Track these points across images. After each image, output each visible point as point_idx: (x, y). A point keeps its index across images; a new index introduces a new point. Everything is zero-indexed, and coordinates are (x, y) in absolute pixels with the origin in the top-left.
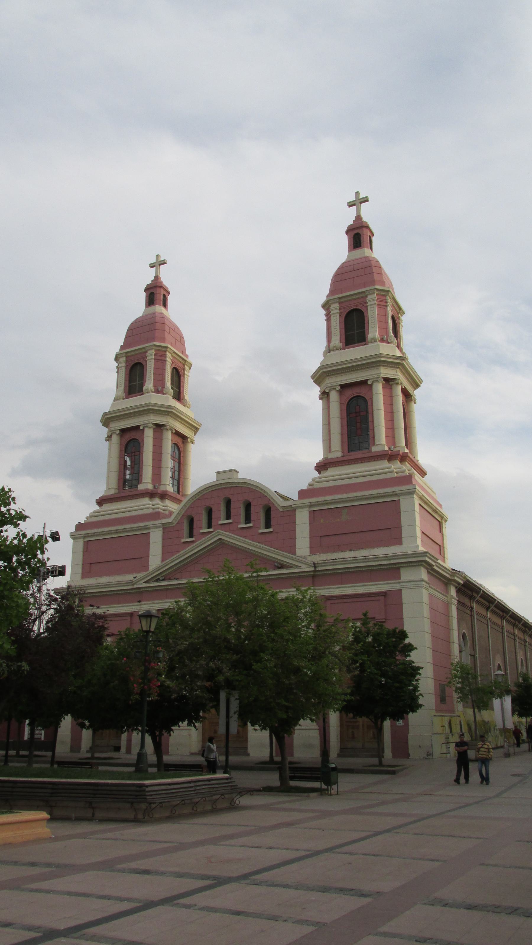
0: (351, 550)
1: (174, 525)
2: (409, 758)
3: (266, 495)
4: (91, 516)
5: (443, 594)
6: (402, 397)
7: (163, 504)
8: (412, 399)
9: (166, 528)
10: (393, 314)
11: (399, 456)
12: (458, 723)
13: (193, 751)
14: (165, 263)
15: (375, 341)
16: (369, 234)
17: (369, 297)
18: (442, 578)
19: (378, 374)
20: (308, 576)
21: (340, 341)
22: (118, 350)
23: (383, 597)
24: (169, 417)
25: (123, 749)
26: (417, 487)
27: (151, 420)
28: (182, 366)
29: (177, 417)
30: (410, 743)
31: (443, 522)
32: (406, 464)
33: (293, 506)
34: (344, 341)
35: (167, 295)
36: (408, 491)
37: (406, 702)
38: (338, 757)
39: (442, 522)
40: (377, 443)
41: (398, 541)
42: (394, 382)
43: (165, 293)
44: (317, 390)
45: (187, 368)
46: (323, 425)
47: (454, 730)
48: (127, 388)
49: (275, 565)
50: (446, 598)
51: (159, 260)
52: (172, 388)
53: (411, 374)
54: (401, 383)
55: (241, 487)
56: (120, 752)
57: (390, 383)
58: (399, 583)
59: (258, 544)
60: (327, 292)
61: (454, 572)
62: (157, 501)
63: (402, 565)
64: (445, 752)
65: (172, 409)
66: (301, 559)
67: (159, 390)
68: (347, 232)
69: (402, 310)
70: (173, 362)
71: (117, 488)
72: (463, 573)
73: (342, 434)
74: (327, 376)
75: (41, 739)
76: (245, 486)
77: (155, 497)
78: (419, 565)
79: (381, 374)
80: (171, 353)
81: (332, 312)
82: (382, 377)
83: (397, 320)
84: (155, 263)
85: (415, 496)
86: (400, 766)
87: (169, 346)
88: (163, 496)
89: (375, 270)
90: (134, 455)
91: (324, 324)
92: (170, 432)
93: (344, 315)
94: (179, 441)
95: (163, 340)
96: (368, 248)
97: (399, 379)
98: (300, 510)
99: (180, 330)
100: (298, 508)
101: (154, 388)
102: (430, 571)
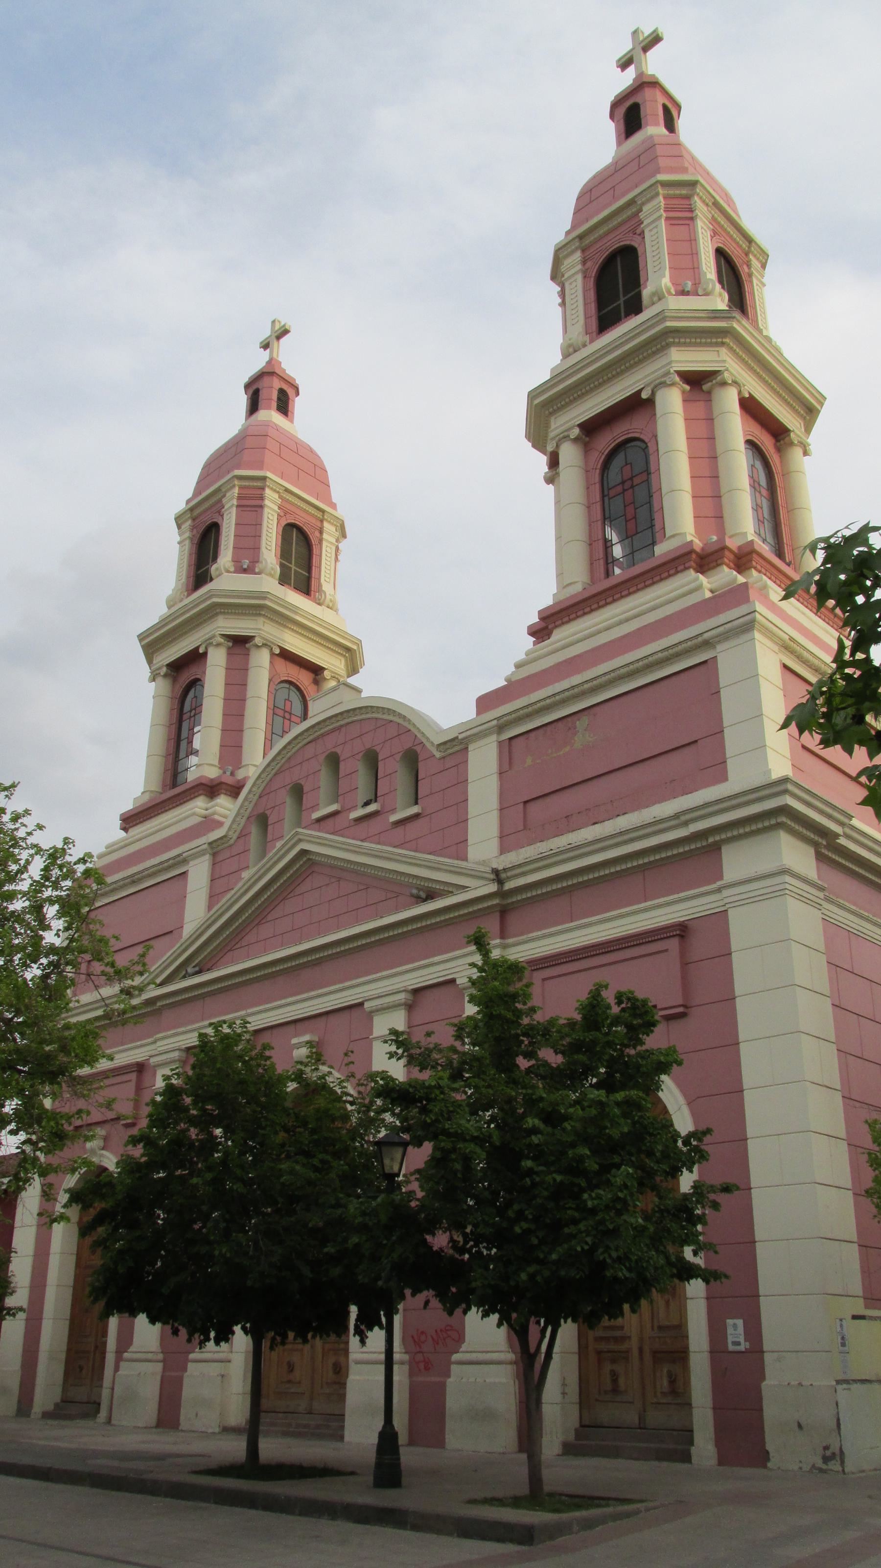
1: (232, 841)
2: (765, 1467)
3: (391, 718)
8: (791, 440)
9: (216, 850)
22: (181, 506)
24: (262, 619)
26: (759, 607)
28: (319, 524)
29: (283, 619)
32: (752, 573)
33: (460, 737)
35: (290, 392)
38: (564, 1454)
42: (714, 382)
49: (412, 895)
53: (802, 394)
57: (705, 387)
58: (719, 890)
63: (723, 836)
65: (265, 598)
67: (245, 566)
69: (756, 243)
80: (278, 492)
82: (675, 371)
86: (604, 1500)
87: (269, 474)
97: (727, 370)
99: (318, 456)
101: (234, 566)
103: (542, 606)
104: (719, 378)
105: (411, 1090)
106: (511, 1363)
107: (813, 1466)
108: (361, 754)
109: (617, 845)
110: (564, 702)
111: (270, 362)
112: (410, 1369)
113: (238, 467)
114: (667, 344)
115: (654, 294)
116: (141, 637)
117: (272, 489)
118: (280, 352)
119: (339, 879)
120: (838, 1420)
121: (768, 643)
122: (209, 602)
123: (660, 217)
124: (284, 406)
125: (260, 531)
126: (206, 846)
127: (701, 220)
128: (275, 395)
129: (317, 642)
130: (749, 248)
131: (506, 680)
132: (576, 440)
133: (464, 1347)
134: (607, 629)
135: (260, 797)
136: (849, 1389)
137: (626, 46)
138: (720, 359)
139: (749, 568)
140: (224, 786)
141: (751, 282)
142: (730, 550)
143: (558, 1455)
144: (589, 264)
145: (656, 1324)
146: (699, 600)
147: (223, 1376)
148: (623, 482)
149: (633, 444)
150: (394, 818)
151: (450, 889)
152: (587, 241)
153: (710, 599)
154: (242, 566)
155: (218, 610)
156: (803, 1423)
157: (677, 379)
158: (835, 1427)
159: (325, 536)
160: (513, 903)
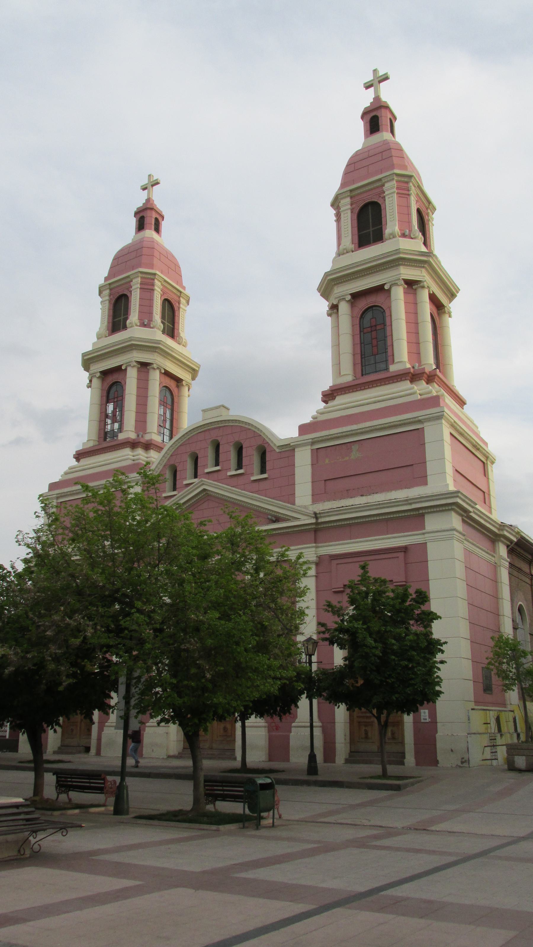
0: (362, 495)
2: (437, 766)
3: (250, 427)
4: (66, 473)
5: (487, 553)
6: (430, 304)
7: (146, 455)
10: (418, 207)
11: (425, 375)
12: (511, 720)
13: (171, 753)
14: (158, 183)
15: (394, 237)
16: (389, 116)
17: (386, 185)
18: (486, 532)
19: (397, 275)
20: (308, 531)
21: (352, 241)
22: (102, 281)
23: (403, 553)
24: (156, 354)
25: (93, 751)
26: (446, 410)
27: (134, 357)
28: (178, 299)
29: (166, 354)
30: (439, 745)
31: (489, 463)
33: (291, 444)
34: (356, 241)
35: (160, 219)
36: (434, 415)
37: (416, 687)
39: (487, 464)
40: (396, 361)
41: (423, 480)
43: (158, 217)
44: (324, 305)
45: (183, 301)
47: (504, 729)
48: (111, 324)
49: (268, 519)
50: (493, 558)
51: (152, 180)
52: (162, 322)
53: (448, 285)
54: (428, 287)
55: (232, 426)
56: (90, 754)
57: (414, 287)
58: (424, 534)
59: (251, 494)
60: (338, 185)
61: (502, 526)
62: (140, 451)
63: (427, 511)
64: (489, 757)
65: (159, 344)
66: (303, 509)
67: (146, 323)
68: (362, 118)
69: (432, 204)
70: (163, 293)
71: (97, 440)
72: (516, 527)
73: (354, 355)
74: (335, 284)
75: (5, 736)
76: (236, 424)
77: (137, 447)
78: (449, 510)
79: (401, 275)
80: (161, 282)
81: (342, 209)
82: (402, 279)
83: (425, 216)
84: (147, 184)
85: (443, 421)
86: (411, 777)
87: (158, 272)
88: (148, 446)
89: (394, 153)
90: (117, 401)
91: (334, 225)
92: (158, 372)
93: (357, 211)
94: (172, 384)
95: (152, 266)
96: (387, 131)
97: (425, 281)
98: (300, 449)
99: (175, 258)
100: (299, 446)
102: (465, 519)
105: (350, 629)
111: (148, 200)
112: (268, 729)
113: (140, 266)
114: (399, 264)
115: (391, 234)
117: (158, 280)
118: (153, 195)
120: (468, 748)
121: (446, 424)
122: (130, 343)
125: (153, 303)
127: (413, 196)
128: (153, 222)
129: (179, 365)
131: (312, 418)
135: (171, 456)
140: (141, 444)
142: (426, 374)
147: (167, 733)
149: (378, 308)
151: (289, 518)
154: (144, 323)
155: (134, 348)
157: (403, 282)
159: (181, 306)
160: (321, 528)
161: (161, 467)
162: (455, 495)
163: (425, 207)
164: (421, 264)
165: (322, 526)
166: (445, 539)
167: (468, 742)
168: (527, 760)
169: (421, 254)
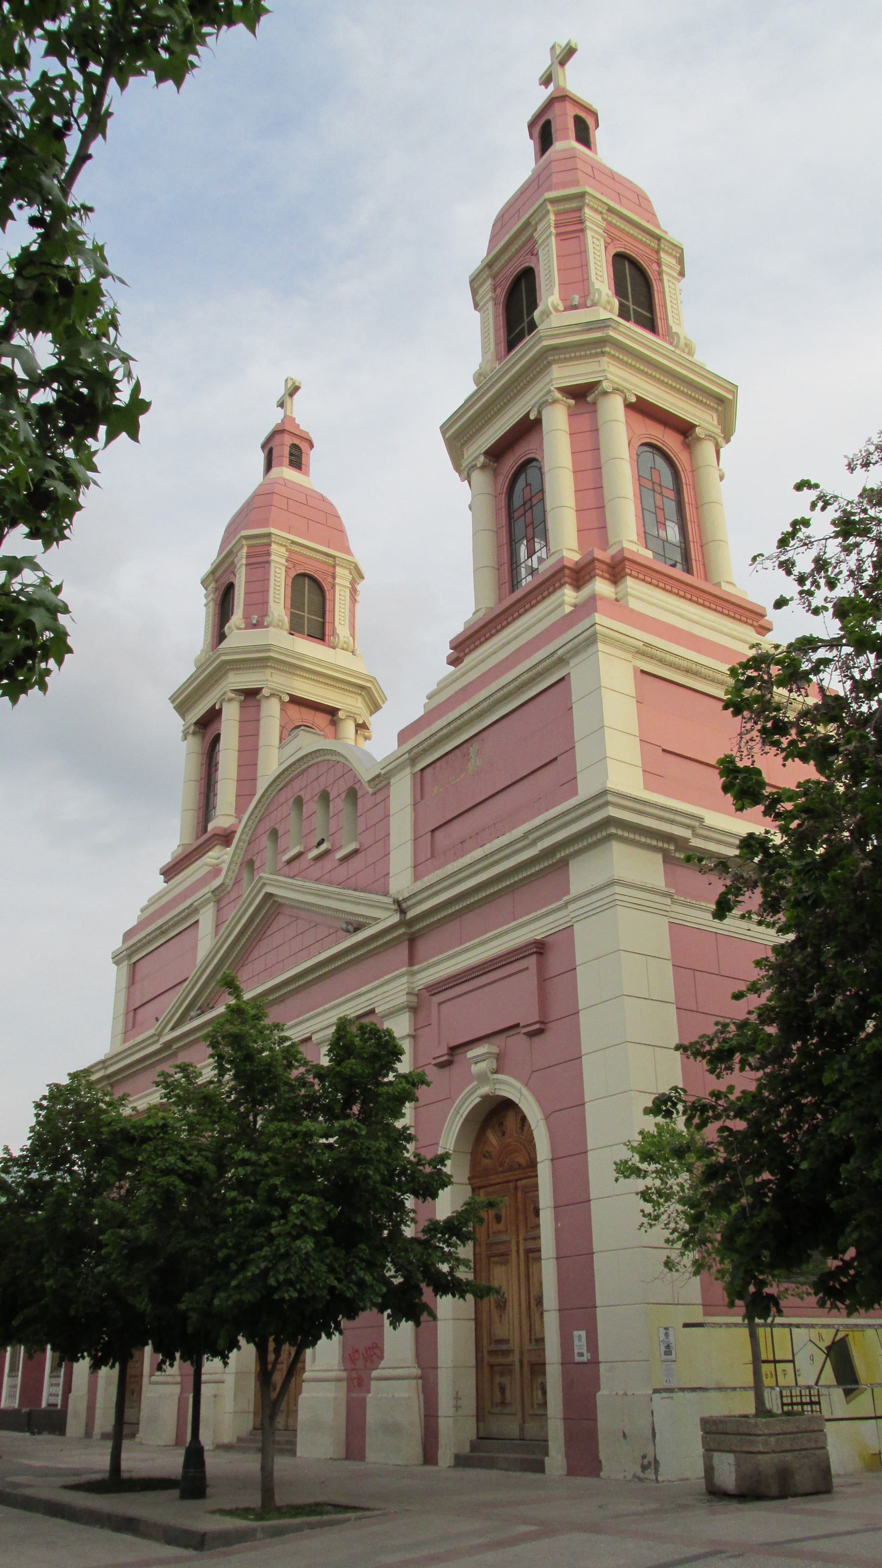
1: (229, 888)
18: (478, 853)
24: (269, 671)
28: (331, 570)
29: (291, 668)
33: (383, 772)
35: (304, 446)
46: (475, 570)
57: (589, 399)
65: (269, 650)
67: (254, 622)
74: (462, 445)
80: (285, 546)
86: (368, 1509)
87: (273, 530)
103: (452, 636)
104: (600, 388)
105: (132, 1131)
106: (416, 1378)
107: (635, 1476)
108: (317, 797)
109: (485, 868)
110: (458, 730)
116: (173, 699)
119: (297, 918)
120: (653, 1429)
123: (550, 235)
124: (297, 460)
126: (209, 895)
128: (286, 451)
130: (659, 245)
132: (483, 467)
133: (383, 1364)
134: (494, 653)
136: (672, 1398)
137: (544, 62)
138: (601, 369)
139: (624, 576)
141: (661, 280)
142: (568, 568)
143: (450, 1467)
144: (499, 290)
145: (533, 1337)
146: (562, 615)
148: (525, 504)
150: (339, 855)
152: (496, 269)
153: (571, 612)
156: (627, 1434)
157: (558, 395)
158: (650, 1436)
159: (338, 581)
161: (237, 869)
162: (600, 802)
163: (652, 249)
164: (596, 349)
165: (421, 925)
166: (605, 907)
167: (652, 1412)
168: (738, 1465)
169: (585, 328)
